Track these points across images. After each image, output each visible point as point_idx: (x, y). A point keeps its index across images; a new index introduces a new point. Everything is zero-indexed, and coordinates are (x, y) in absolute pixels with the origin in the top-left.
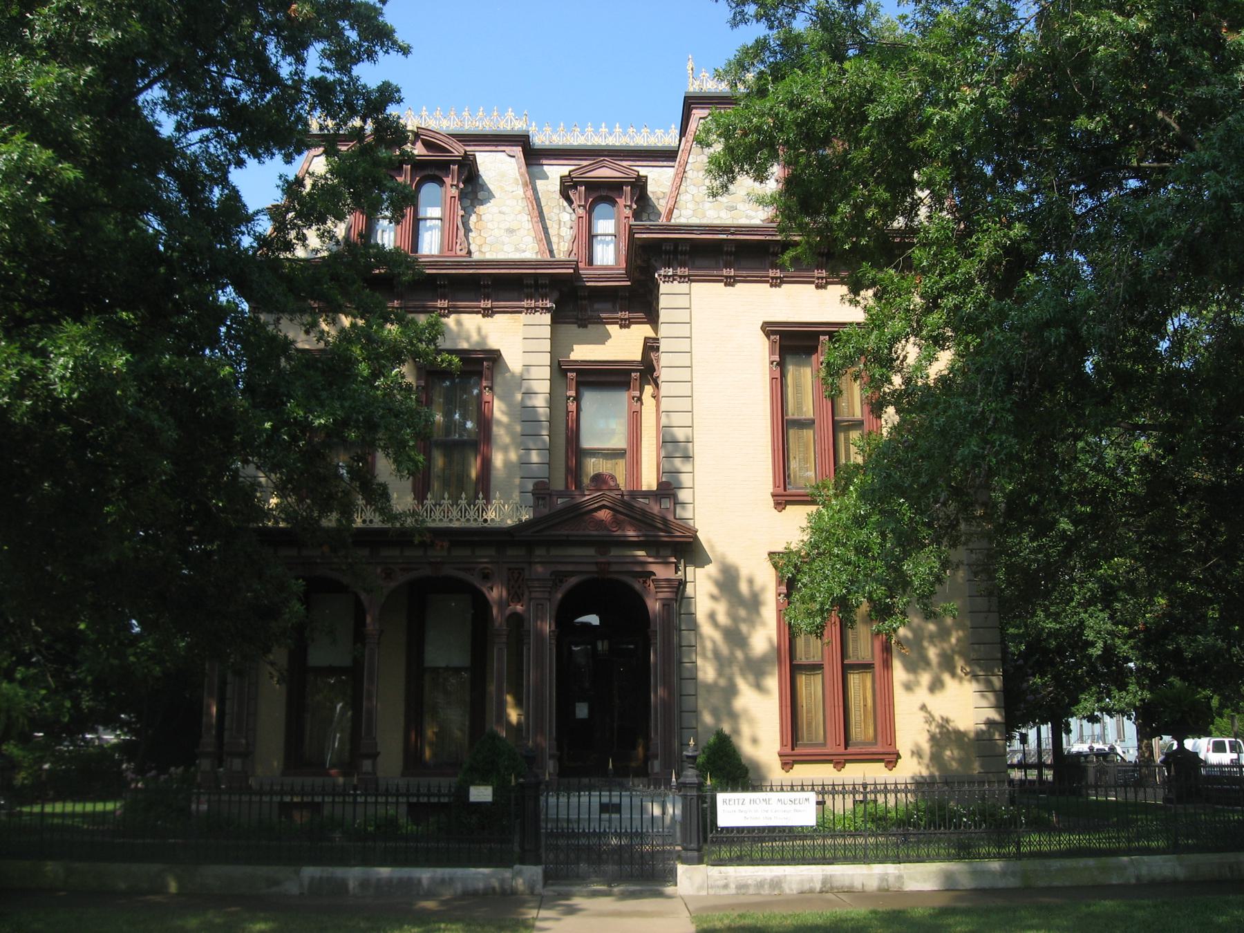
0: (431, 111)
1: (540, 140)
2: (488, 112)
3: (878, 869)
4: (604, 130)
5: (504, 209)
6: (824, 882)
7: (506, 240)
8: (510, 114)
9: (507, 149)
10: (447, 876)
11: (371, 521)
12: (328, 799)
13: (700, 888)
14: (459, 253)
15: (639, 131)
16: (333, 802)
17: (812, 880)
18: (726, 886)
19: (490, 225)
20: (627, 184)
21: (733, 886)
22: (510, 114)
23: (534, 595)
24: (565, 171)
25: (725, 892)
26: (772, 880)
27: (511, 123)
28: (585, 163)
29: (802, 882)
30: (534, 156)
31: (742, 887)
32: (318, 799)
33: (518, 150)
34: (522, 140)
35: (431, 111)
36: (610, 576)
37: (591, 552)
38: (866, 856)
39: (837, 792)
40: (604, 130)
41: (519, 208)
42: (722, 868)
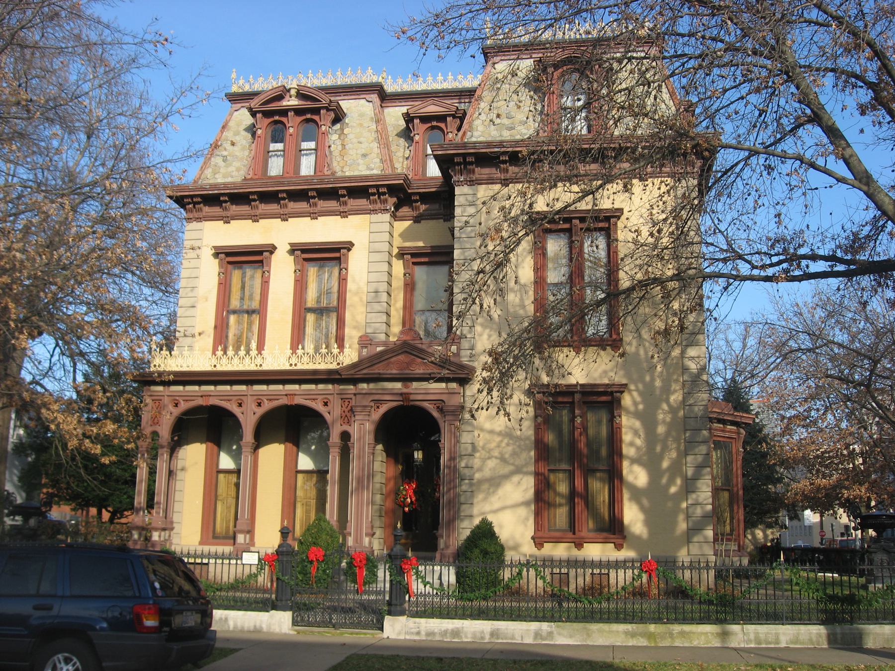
0: (315, 73)
1: (390, 87)
2: (354, 71)
3: (534, 626)
4: (440, 78)
5: (362, 139)
6: (492, 634)
7: (361, 161)
8: (370, 71)
9: (367, 97)
10: (223, 617)
11: (159, 366)
12: (212, 561)
13: (399, 633)
14: (326, 173)
15: (465, 77)
16: (230, 564)
17: (483, 632)
18: (418, 633)
19: (351, 152)
20: (449, 115)
21: (423, 633)
22: (370, 71)
23: (357, 417)
24: (404, 110)
25: (417, 638)
26: (452, 630)
27: (369, 77)
28: (417, 103)
29: (474, 634)
30: (385, 97)
31: (430, 634)
32: (205, 561)
33: (375, 97)
34: (378, 90)
35: (315, 73)
36: (412, 403)
37: (398, 385)
38: (553, 616)
39: (695, 568)
40: (440, 78)
41: (372, 139)
42: (417, 620)
